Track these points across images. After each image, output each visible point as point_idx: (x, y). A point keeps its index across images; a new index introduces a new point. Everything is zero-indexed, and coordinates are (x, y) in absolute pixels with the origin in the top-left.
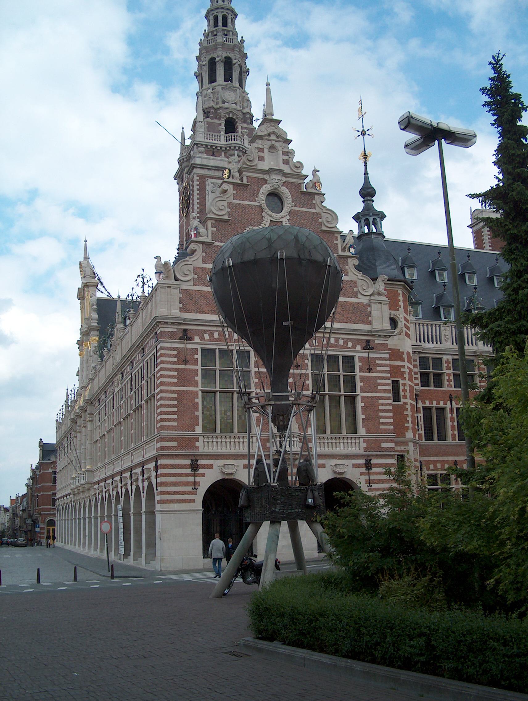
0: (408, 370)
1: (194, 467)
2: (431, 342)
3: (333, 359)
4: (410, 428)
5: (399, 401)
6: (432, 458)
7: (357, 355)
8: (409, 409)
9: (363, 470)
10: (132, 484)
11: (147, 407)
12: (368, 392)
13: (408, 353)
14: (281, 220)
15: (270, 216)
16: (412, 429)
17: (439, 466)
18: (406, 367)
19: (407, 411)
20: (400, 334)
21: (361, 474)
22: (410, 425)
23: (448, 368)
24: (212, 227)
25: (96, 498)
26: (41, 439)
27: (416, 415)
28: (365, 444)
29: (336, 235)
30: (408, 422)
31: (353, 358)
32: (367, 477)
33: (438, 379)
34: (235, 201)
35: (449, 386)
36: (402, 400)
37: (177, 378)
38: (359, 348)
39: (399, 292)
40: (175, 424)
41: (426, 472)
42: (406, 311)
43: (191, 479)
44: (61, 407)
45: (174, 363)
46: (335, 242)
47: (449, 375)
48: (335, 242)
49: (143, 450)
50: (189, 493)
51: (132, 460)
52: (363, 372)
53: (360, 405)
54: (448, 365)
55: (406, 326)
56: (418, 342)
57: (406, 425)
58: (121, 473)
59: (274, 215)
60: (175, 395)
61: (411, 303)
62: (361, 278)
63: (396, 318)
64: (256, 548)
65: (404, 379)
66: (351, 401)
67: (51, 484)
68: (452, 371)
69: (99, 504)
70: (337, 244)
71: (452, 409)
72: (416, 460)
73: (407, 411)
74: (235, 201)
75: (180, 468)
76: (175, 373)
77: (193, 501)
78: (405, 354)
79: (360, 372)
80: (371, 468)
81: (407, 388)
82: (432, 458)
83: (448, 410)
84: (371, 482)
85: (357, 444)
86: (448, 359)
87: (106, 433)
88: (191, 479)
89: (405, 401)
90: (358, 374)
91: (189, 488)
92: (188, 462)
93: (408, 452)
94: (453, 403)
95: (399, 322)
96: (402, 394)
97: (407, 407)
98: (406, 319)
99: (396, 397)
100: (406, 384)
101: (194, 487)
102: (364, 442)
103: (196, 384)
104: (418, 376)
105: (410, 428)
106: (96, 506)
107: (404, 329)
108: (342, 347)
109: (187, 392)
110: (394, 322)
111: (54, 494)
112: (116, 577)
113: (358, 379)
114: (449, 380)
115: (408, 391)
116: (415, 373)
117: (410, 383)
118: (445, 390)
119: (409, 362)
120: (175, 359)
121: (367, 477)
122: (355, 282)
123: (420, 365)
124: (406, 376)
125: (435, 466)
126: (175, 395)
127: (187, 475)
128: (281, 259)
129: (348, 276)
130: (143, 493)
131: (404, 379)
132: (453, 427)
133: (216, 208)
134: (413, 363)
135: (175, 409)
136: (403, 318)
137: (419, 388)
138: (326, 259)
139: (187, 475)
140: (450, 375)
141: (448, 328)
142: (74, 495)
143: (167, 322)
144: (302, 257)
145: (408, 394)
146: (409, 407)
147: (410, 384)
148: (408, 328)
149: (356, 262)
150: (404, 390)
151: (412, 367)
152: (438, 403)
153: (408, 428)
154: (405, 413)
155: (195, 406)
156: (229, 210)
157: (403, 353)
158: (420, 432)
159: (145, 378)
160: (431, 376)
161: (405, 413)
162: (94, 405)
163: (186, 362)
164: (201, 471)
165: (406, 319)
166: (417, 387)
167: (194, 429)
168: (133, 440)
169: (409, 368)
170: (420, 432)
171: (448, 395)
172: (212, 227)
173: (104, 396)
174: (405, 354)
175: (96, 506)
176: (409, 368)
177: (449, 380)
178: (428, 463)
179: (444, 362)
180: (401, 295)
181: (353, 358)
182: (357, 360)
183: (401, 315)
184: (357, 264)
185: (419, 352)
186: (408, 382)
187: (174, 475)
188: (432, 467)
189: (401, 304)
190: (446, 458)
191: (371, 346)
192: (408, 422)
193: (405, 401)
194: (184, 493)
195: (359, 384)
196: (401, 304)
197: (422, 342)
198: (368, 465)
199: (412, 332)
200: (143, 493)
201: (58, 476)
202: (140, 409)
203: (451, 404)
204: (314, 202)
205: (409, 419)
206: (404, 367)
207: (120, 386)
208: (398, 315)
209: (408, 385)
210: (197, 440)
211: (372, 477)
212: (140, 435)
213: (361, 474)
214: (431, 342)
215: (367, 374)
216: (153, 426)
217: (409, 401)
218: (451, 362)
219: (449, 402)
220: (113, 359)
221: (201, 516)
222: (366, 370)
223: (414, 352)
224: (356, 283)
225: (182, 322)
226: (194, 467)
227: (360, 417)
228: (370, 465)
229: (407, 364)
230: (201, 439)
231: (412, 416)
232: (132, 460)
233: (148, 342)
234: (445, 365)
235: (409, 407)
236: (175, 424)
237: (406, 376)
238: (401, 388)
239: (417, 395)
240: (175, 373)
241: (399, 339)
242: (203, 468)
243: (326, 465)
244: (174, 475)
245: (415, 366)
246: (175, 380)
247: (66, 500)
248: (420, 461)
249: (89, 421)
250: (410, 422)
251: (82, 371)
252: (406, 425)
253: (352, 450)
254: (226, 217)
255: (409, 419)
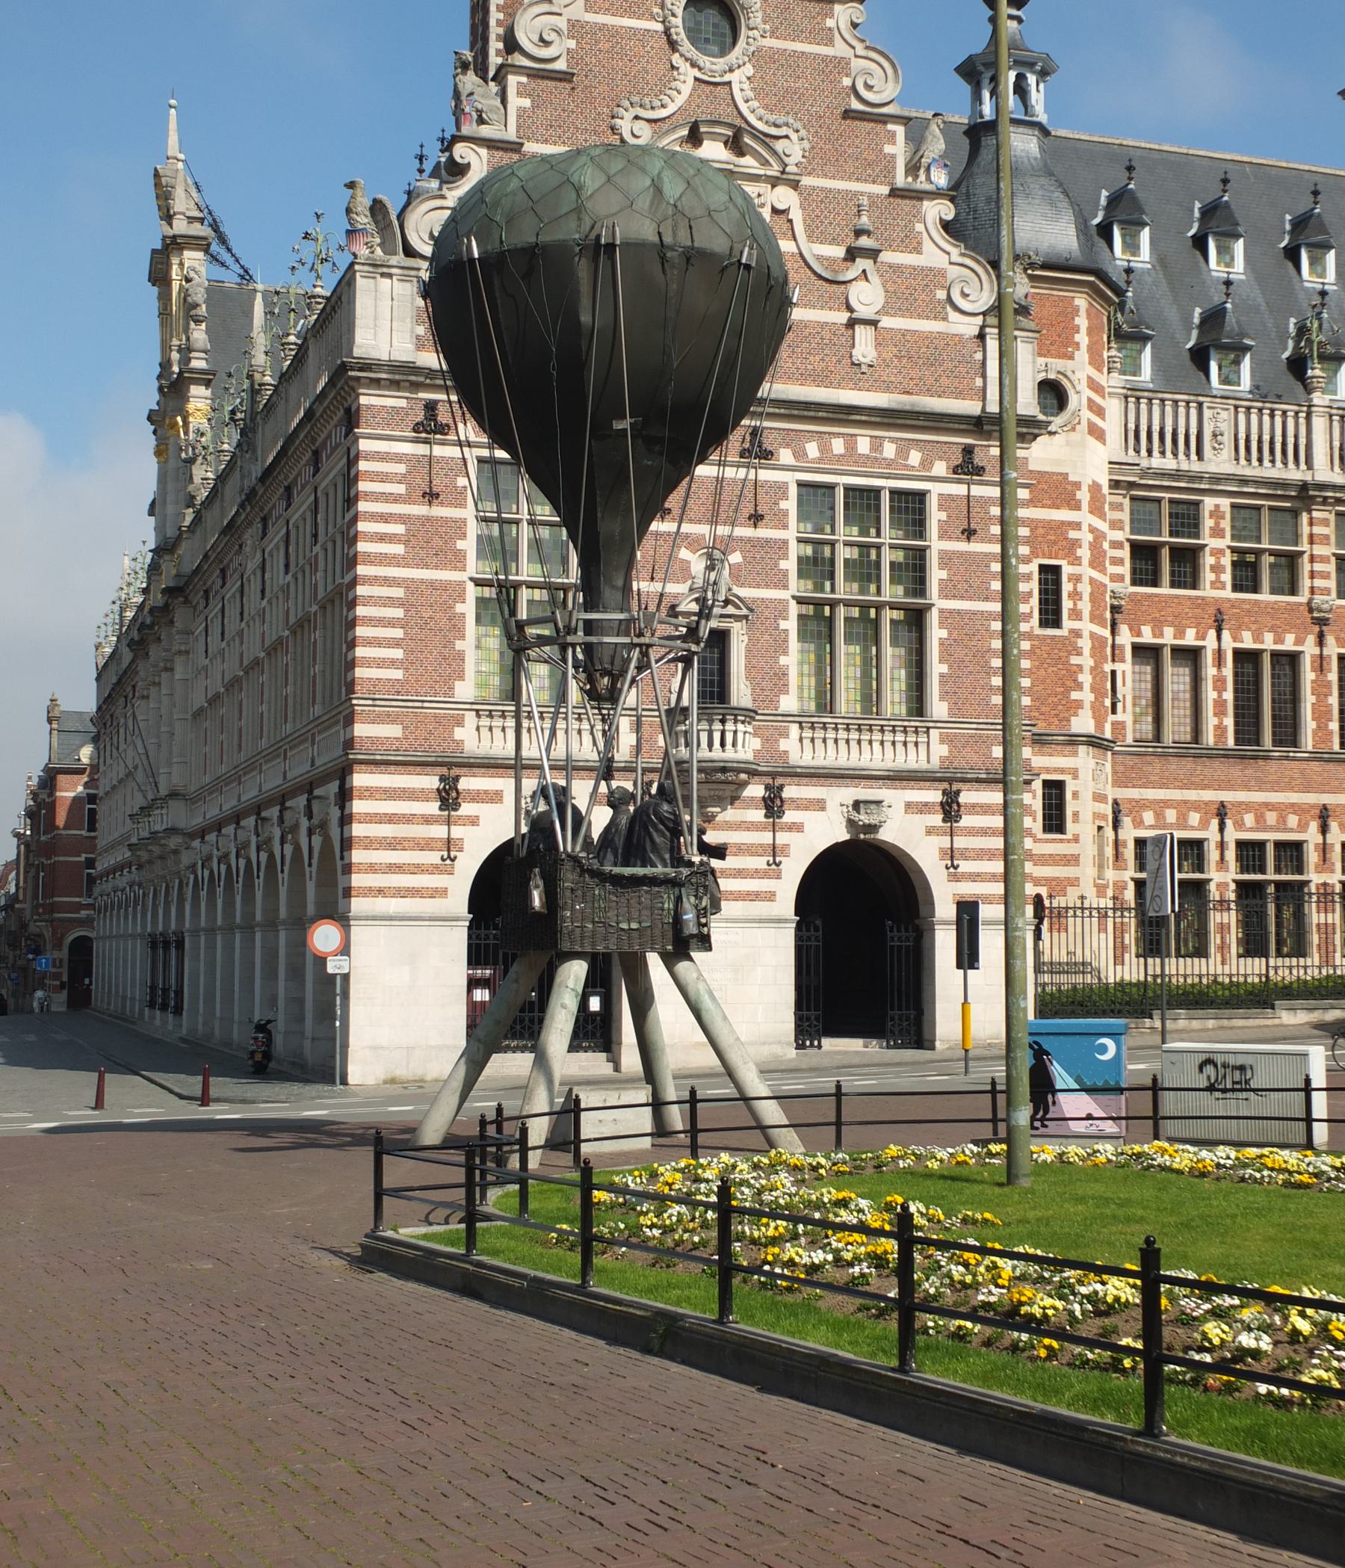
0: (1090, 537)
1: (449, 798)
2: (1169, 453)
3: (862, 501)
4: (1087, 705)
5: (1057, 623)
6: (1151, 794)
7: (935, 489)
8: (1087, 651)
9: (937, 819)
10: (283, 842)
11: (324, 623)
12: (962, 598)
13: (1095, 488)
14: (727, 78)
15: (694, 65)
16: (1093, 707)
17: (1271, 818)
18: (1085, 527)
19: (1079, 654)
20: (1073, 429)
21: (930, 831)
22: (1086, 696)
23: (1218, 532)
24: (519, 94)
25: (196, 877)
26: (1339, 93)
27: (1108, 667)
28: (782, 748)
29: (890, 127)
30: (1079, 687)
31: (921, 496)
32: (945, 842)
33: (1187, 564)
34: (590, 17)
35: (1216, 583)
36: (1067, 623)
37: (406, 543)
38: (940, 468)
39: (1077, 302)
40: (398, 674)
41: (1129, 833)
42: (1095, 361)
43: (439, 831)
44: (108, 607)
45: (396, 499)
46: (888, 149)
47: (1217, 553)
48: (888, 149)
49: (313, 744)
50: (433, 870)
51: (285, 773)
52: (950, 538)
53: (936, 633)
54: (1217, 524)
55: (1092, 405)
56: (1131, 452)
57: (1075, 695)
58: (257, 809)
59: (704, 60)
60: (398, 593)
61: (1119, 335)
62: (960, 260)
63: (1065, 382)
64: (553, 1018)
65: (1076, 561)
66: (916, 619)
67: (84, 833)
68: (1227, 541)
69: (203, 894)
70: (893, 156)
71: (1219, 654)
72: (1099, 798)
73: (1079, 654)
74: (590, 17)
75: (409, 799)
76: (399, 529)
77: (442, 892)
78: (1085, 488)
79: (941, 538)
80: (456, 806)
81: (1085, 588)
82: (1151, 794)
83: (1209, 658)
84: (956, 854)
85: (922, 748)
86: (1217, 506)
87: (222, 690)
88: (439, 831)
89: (1076, 625)
90: (936, 544)
91: (434, 857)
92: (430, 782)
93: (1075, 773)
94: (1226, 635)
95: (1071, 393)
96: (1067, 604)
97: (1080, 643)
98: (1094, 386)
99: (1051, 615)
100: (1079, 578)
101: (445, 854)
102: (942, 742)
103: (458, 560)
104: (1125, 553)
105: (1087, 705)
106: (196, 898)
107: (1086, 414)
108: (890, 463)
109: (433, 585)
110: (1054, 393)
111: (90, 863)
112: (218, 1100)
113: (933, 560)
114: (1217, 569)
115: (1086, 597)
116: (1116, 545)
117: (1095, 574)
118: (1203, 598)
119: (1097, 509)
120: (401, 489)
121: (945, 842)
122: (942, 273)
123: (1132, 521)
124: (1084, 553)
125: (1260, 818)
126: (398, 593)
127: (427, 820)
128: (607, 245)
129: (920, 253)
130: (310, 865)
131: (1076, 561)
132: (1220, 705)
133: (536, 38)
134: (1111, 515)
135: (399, 633)
136: (1084, 382)
137: (1127, 588)
138: (737, 247)
139: (427, 820)
140: (1221, 552)
141: (1224, 415)
142: (140, 867)
143: (378, 380)
144: (668, 239)
145: (1085, 606)
146: (1085, 644)
147: (1100, 570)
148: (1100, 412)
149: (945, 210)
150: (1075, 595)
151: (1102, 526)
152: (1180, 633)
153: (1079, 704)
154: (1074, 660)
155: (454, 626)
156: (572, 44)
157: (1078, 485)
158: (1120, 717)
159: (321, 538)
160: (1165, 553)
161: (1074, 660)
162: (195, 608)
163: (431, 496)
164: (466, 809)
165: (1094, 386)
166: (1117, 586)
167: (452, 689)
168: (290, 715)
169: (1092, 530)
170: (1120, 717)
171: (1212, 611)
172: (519, 94)
173: (219, 582)
174: (1085, 488)
175: (196, 898)
176: (1092, 530)
177: (1217, 569)
178: (1141, 805)
179: (1207, 514)
180: (1083, 312)
181: (921, 496)
182: (933, 503)
183: (1079, 372)
184: (950, 217)
185: (1132, 485)
186: (1087, 572)
187: (391, 819)
188: (1149, 817)
189: (1082, 338)
190: (1192, 795)
191: (977, 461)
192: (1079, 687)
193: (1076, 625)
194: (418, 869)
195: (936, 575)
196: (1082, 338)
197: (1144, 452)
198: (950, 809)
199: (1113, 423)
200: (310, 865)
201: (102, 809)
202: (306, 625)
203: (1219, 638)
204: (830, 23)
205: (1086, 678)
206: (1077, 526)
207: (259, 555)
208: (1069, 374)
209: (1086, 580)
210: (460, 722)
211: (960, 842)
212: (305, 699)
213: (930, 831)
214: (1169, 453)
215: (962, 546)
216: (336, 678)
217: (1087, 626)
218: (1228, 516)
219: (1212, 633)
220: (243, 477)
221: (463, 934)
222: (959, 532)
223: (1115, 484)
224: (944, 276)
225: (421, 379)
226: (449, 798)
227: (936, 668)
228: (955, 807)
229: (1085, 517)
230: (470, 718)
231: (1096, 670)
232: (285, 773)
233: (329, 436)
234: (1208, 523)
235: (1085, 644)
236: (398, 674)
237: (1084, 553)
238: (1066, 587)
239: (1115, 609)
240: (399, 529)
241: (1068, 443)
242: (473, 800)
243: (829, 804)
244: (391, 819)
245: (1116, 525)
246: (399, 549)
247: (122, 880)
248: (1116, 802)
249: (180, 652)
250: (1087, 686)
251: (165, 503)
252: (1075, 695)
253: (913, 760)
254: (561, 65)
255: (1086, 678)
